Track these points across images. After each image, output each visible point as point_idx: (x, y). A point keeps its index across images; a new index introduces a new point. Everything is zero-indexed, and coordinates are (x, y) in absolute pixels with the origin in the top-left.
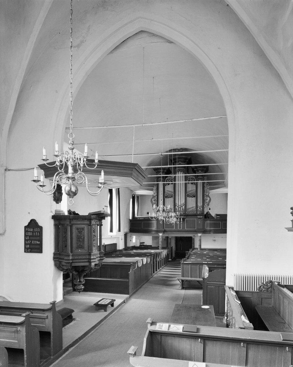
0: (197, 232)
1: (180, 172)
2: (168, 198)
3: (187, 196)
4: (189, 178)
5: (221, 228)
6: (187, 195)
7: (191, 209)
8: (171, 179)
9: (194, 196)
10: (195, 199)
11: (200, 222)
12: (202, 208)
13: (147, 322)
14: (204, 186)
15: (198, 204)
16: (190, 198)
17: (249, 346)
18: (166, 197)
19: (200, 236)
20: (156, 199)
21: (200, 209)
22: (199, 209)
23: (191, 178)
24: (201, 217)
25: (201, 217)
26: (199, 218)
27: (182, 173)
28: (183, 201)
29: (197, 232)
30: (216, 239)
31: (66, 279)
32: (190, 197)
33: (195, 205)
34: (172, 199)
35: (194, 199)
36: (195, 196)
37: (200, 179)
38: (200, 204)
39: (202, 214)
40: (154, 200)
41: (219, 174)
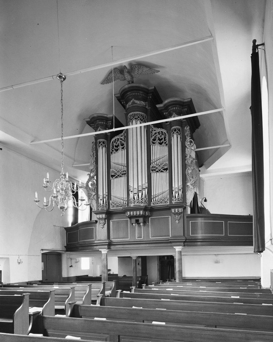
0: (171, 242)
1: (134, 121)
2: (117, 177)
3: (152, 170)
4: (156, 133)
5: (226, 232)
6: (150, 169)
7: (160, 197)
8: (121, 139)
9: (164, 169)
10: (168, 174)
11: (177, 221)
12: (180, 193)
13: (256, 44)
14: (186, 146)
15: (173, 186)
16: (158, 174)
17: (131, 219)
18: (112, 176)
19: (180, 252)
20: (95, 182)
21: (177, 195)
22: (177, 194)
23: (159, 132)
24: (178, 211)
25: (178, 211)
26: (175, 214)
27: (139, 122)
28: (144, 182)
29: (171, 242)
30: (220, 258)
31: (160, 259)
32: (157, 171)
33: (167, 188)
34: (123, 179)
35: (166, 175)
36: (166, 169)
37: (175, 130)
38: (177, 184)
39: (182, 205)
40: (92, 185)
41: (168, 225)
